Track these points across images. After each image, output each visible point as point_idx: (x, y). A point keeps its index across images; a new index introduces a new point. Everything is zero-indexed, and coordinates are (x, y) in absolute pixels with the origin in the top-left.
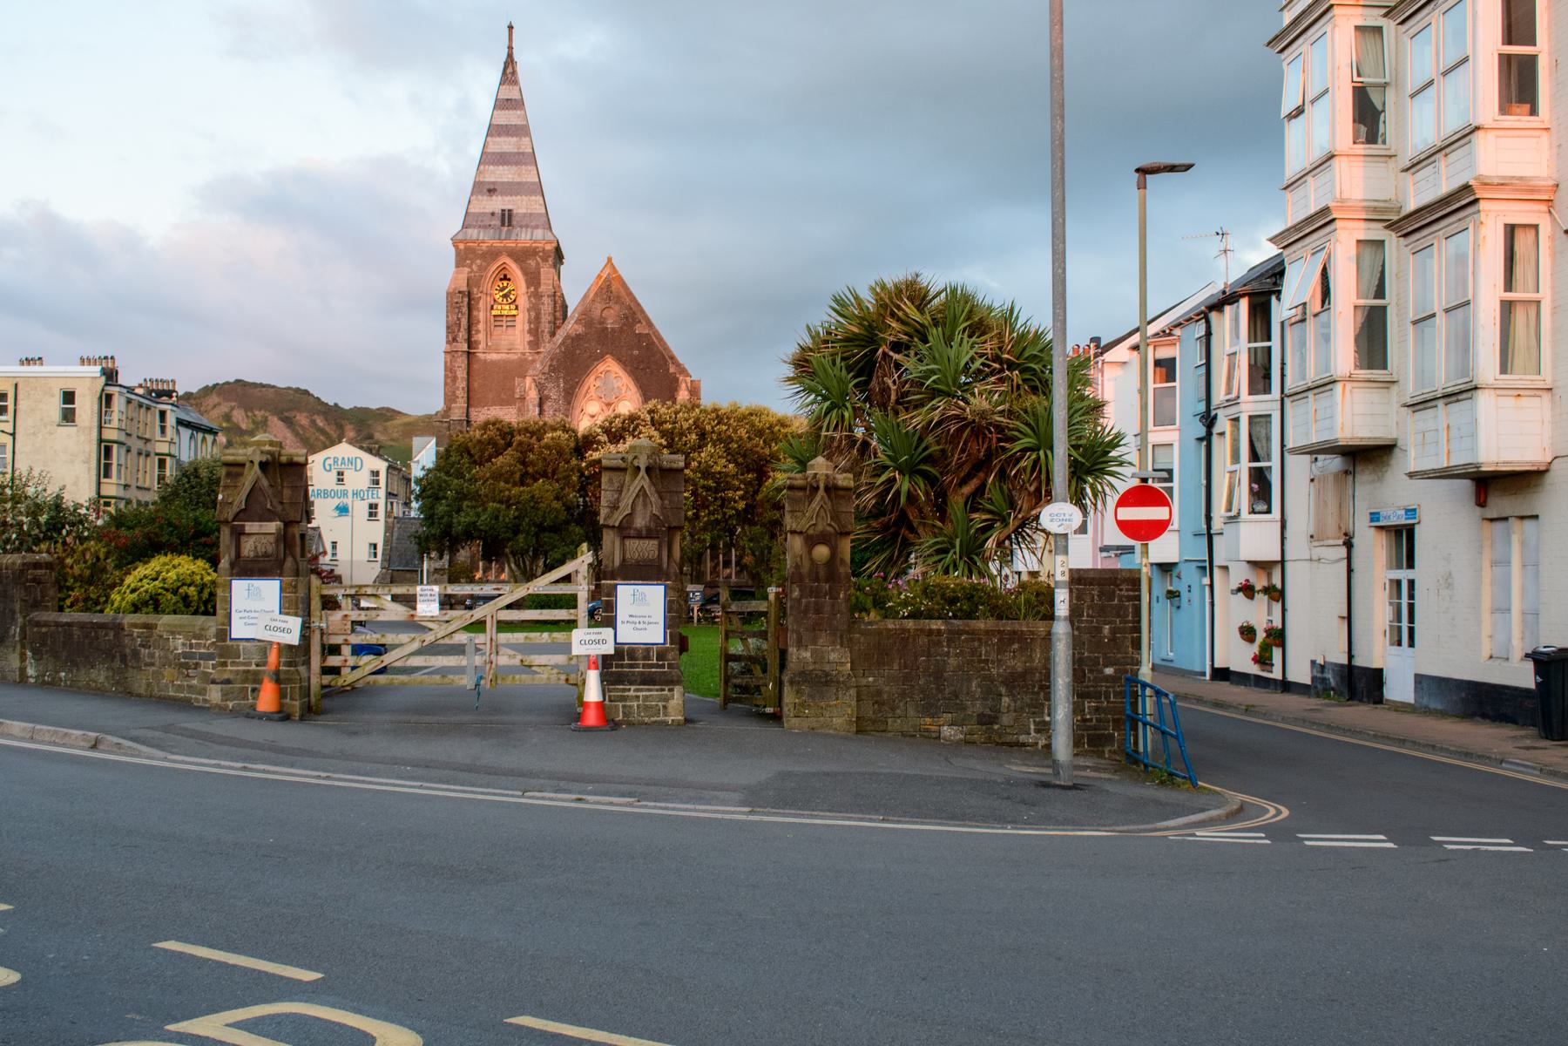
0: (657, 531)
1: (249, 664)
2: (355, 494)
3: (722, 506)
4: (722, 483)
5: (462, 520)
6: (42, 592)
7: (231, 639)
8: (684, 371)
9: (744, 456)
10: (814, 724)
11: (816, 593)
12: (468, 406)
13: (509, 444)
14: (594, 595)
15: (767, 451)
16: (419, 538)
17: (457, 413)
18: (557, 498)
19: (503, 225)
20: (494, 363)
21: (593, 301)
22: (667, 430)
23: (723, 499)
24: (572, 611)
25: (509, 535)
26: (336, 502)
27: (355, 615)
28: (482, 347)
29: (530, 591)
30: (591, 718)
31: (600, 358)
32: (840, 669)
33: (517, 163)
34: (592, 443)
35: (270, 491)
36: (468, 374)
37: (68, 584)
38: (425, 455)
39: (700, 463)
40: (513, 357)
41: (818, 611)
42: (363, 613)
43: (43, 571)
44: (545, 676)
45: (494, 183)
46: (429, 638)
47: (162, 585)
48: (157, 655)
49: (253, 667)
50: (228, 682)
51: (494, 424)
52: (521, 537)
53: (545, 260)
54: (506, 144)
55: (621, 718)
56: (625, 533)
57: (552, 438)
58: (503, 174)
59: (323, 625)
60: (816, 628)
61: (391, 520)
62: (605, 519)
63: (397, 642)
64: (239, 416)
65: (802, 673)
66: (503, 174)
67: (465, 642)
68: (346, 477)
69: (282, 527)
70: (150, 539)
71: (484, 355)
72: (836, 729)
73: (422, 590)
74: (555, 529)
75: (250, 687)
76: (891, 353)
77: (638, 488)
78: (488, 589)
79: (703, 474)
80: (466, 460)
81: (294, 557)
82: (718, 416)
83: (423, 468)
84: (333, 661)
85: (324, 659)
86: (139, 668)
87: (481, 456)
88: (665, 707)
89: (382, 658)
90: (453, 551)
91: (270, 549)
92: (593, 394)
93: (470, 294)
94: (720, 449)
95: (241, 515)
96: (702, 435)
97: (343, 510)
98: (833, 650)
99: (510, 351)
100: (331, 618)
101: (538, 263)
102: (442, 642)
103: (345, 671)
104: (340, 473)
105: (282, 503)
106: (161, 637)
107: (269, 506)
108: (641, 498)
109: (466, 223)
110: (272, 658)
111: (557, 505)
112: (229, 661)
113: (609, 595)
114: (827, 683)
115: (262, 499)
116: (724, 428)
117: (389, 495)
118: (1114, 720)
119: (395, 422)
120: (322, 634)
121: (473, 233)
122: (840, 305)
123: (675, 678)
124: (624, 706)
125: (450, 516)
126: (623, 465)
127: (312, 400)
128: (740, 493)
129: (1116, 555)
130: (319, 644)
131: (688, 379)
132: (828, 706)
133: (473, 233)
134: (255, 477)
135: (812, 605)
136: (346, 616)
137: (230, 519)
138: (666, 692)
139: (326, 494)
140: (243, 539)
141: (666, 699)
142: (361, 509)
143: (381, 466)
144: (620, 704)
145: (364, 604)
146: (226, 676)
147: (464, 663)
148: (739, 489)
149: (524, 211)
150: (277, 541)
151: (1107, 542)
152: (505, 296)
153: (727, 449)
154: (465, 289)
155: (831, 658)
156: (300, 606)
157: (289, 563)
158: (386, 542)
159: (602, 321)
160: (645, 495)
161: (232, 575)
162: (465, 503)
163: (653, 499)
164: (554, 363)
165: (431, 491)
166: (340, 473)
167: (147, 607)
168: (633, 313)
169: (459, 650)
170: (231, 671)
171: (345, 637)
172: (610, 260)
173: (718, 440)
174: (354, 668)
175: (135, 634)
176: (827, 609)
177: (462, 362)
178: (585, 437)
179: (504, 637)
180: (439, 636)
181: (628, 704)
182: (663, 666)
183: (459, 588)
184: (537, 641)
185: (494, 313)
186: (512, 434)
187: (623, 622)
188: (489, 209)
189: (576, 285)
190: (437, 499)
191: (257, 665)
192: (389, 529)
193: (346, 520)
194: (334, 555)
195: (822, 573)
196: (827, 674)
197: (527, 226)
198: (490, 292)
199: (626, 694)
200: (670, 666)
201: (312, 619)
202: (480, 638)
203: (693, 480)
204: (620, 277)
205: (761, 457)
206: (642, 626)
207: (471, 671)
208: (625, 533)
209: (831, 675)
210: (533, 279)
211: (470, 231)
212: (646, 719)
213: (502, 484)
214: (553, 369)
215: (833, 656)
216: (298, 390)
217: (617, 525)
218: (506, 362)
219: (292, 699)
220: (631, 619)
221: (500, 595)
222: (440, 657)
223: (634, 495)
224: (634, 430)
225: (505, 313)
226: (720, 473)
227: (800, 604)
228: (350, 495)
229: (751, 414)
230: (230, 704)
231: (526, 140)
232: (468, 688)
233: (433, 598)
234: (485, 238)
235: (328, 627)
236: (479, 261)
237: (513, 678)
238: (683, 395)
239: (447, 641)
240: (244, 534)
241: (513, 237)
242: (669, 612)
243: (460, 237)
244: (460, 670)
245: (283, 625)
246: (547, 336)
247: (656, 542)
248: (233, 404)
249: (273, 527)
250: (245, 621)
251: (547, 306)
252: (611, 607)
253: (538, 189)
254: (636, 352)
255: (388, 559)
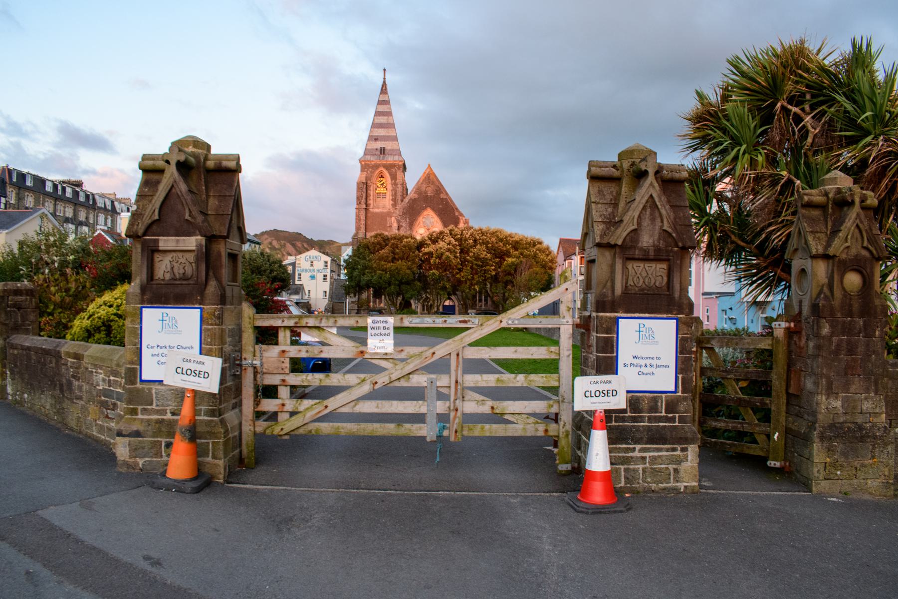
0: (667, 251)
1: (164, 412)
2: (318, 271)
3: (485, 273)
4: (484, 262)
5: (365, 279)
6: (22, 316)
7: (142, 381)
8: (462, 215)
9: (494, 250)
10: (847, 488)
11: (848, 330)
12: (366, 231)
13: (387, 245)
14: (584, 326)
15: (505, 249)
16: (345, 287)
17: (361, 235)
18: (408, 268)
19: (381, 154)
20: (377, 213)
21: (422, 183)
22: (458, 238)
23: (485, 270)
24: (553, 349)
25: (387, 286)
26: (310, 274)
27: (294, 352)
28: (372, 206)
30: (597, 494)
31: (424, 209)
32: (875, 420)
33: (387, 128)
34: (424, 245)
35: (189, 198)
36: (366, 217)
37: (49, 311)
38: (347, 253)
39: (474, 253)
40: (385, 211)
41: (851, 351)
42: (304, 348)
43: (24, 298)
44: (520, 426)
45: (377, 136)
46: (382, 379)
47: (115, 311)
48: (84, 388)
49: (169, 416)
50: (137, 434)
51: (380, 235)
52: (392, 287)
53: (399, 169)
54: (382, 120)
55: (622, 484)
56: (630, 253)
57: (407, 242)
58: (381, 132)
59: (257, 362)
60: (848, 371)
61: (332, 280)
62: (601, 237)
63: (343, 383)
64: (275, 243)
65: (832, 426)
66: (381, 132)
67: (425, 384)
68: (314, 264)
69: (204, 243)
70: (119, 270)
71: (373, 210)
72: (870, 493)
73: (374, 322)
74: (408, 283)
75: (164, 441)
76: (790, 107)
77: (646, 198)
78: (453, 321)
79: (476, 258)
80: (367, 251)
81: (219, 280)
82: (482, 232)
83: (348, 255)
84: (269, 405)
85: (257, 403)
86: (71, 400)
87: (374, 250)
88: (676, 471)
89: (326, 402)
90: (360, 293)
91: (189, 271)
92: (422, 225)
93: (366, 184)
94: (484, 247)
95: (154, 227)
96: (475, 241)
97: (313, 277)
98: (866, 398)
99: (384, 207)
100: (266, 354)
101: (396, 170)
102: (397, 384)
103: (282, 417)
104: (312, 262)
105: (204, 214)
106: (87, 369)
107: (187, 217)
108: (648, 210)
110: (187, 409)
111: (408, 271)
112: (140, 408)
113: (608, 330)
114: (862, 439)
115: (180, 207)
116: (485, 237)
117: (332, 271)
119: (334, 246)
120: (256, 373)
121: (368, 157)
122: (735, 64)
123: (689, 435)
124: (626, 470)
125: (360, 277)
126: (617, 173)
128: (493, 267)
129: (716, 297)
130: (252, 386)
131: (464, 218)
132: (863, 466)
133: (368, 157)
134: (171, 180)
135: (844, 345)
136: (284, 351)
137: (140, 233)
138: (678, 453)
139: (306, 271)
140: (158, 257)
141: (679, 461)
142: (320, 277)
143: (329, 259)
144: (622, 467)
145: (305, 337)
146: (134, 428)
147: (423, 410)
148: (492, 265)
149: (390, 148)
150: (198, 260)
151: (706, 290)
152: (382, 184)
153: (487, 247)
154: (364, 181)
155: (864, 408)
156: (228, 340)
157: (212, 287)
158: (331, 289)
159: (426, 192)
160: (654, 206)
161: (142, 302)
162: (367, 271)
163: (663, 212)
164: (405, 211)
165: (351, 265)
166: (312, 262)
167: (100, 332)
168: (440, 189)
169: (417, 394)
170: (142, 420)
171: (282, 377)
172: (429, 165)
173: (482, 243)
174: (293, 414)
175: (69, 364)
176: (861, 349)
177: (363, 213)
178: (420, 242)
179: (471, 379)
180: (394, 377)
181: (631, 467)
182: (672, 420)
183: (418, 320)
184: (511, 385)
185: (377, 192)
186: (388, 239)
187: (625, 365)
188: (375, 147)
189: (412, 179)
190: (354, 269)
191: (173, 414)
192: (331, 284)
193: (314, 281)
194: (309, 295)
195: (856, 306)
196: (860, 428)
197: (391, 155)
198: (375, 183)
199: (630, 454)
200: (682, 420)
201: (244, 356)
202: (443, 381)
203: (471, 261)
204: (434, 173)
205: (502, 251)
206: (649, 370)
207: (431, 419)
208: (630, 253)
209: (866, 429)
210: (394, 177)
211: (367, 156)
212: (653, 486)
213: (383, 263)
214: (404, 213)
215: (866, 406)
216: (297, 233)
217: (620, 243)
218: (382, 213)
219: (214, 457)
220: (636, 361)
221: (468, 329)
222: (395, 403)
223: (641, 206)
224: (443, 238)
225: (382, 192)
226: (484, 258)
227: (831, 342)
228: (316, 271)
229: (496, 232)
230: (141, 462)
231: (391, 117)
232: (428, 439)
233: (386, 332)
234: (373, 159)
235: (262, 365)
236: (370, 170)
237: (482, 428)
238: (461, 225)
239: (403, 383)
240: (158, 251)
241: (386, 159)
242: (681, 353)
243: (363, 159)
244: (419, 418)
245: (198, 367)
246: (399, 201)
247: (664, 266)
248: (273, 238)
249: (192, 242)
250: (157, 359)
251: (400, 188)
252: (609, 346)
253: (395, 139)
254: (440, 206)
255: (331, 297)
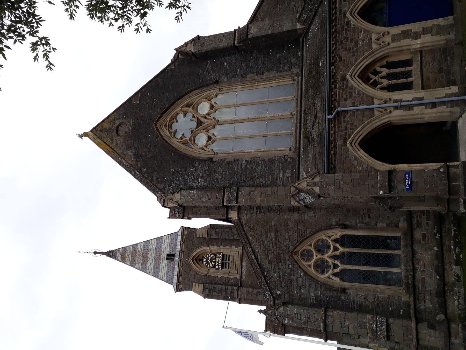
29: (389, 70)
109: (144, 271)
118: (365, 259)
127: (173, 67)
